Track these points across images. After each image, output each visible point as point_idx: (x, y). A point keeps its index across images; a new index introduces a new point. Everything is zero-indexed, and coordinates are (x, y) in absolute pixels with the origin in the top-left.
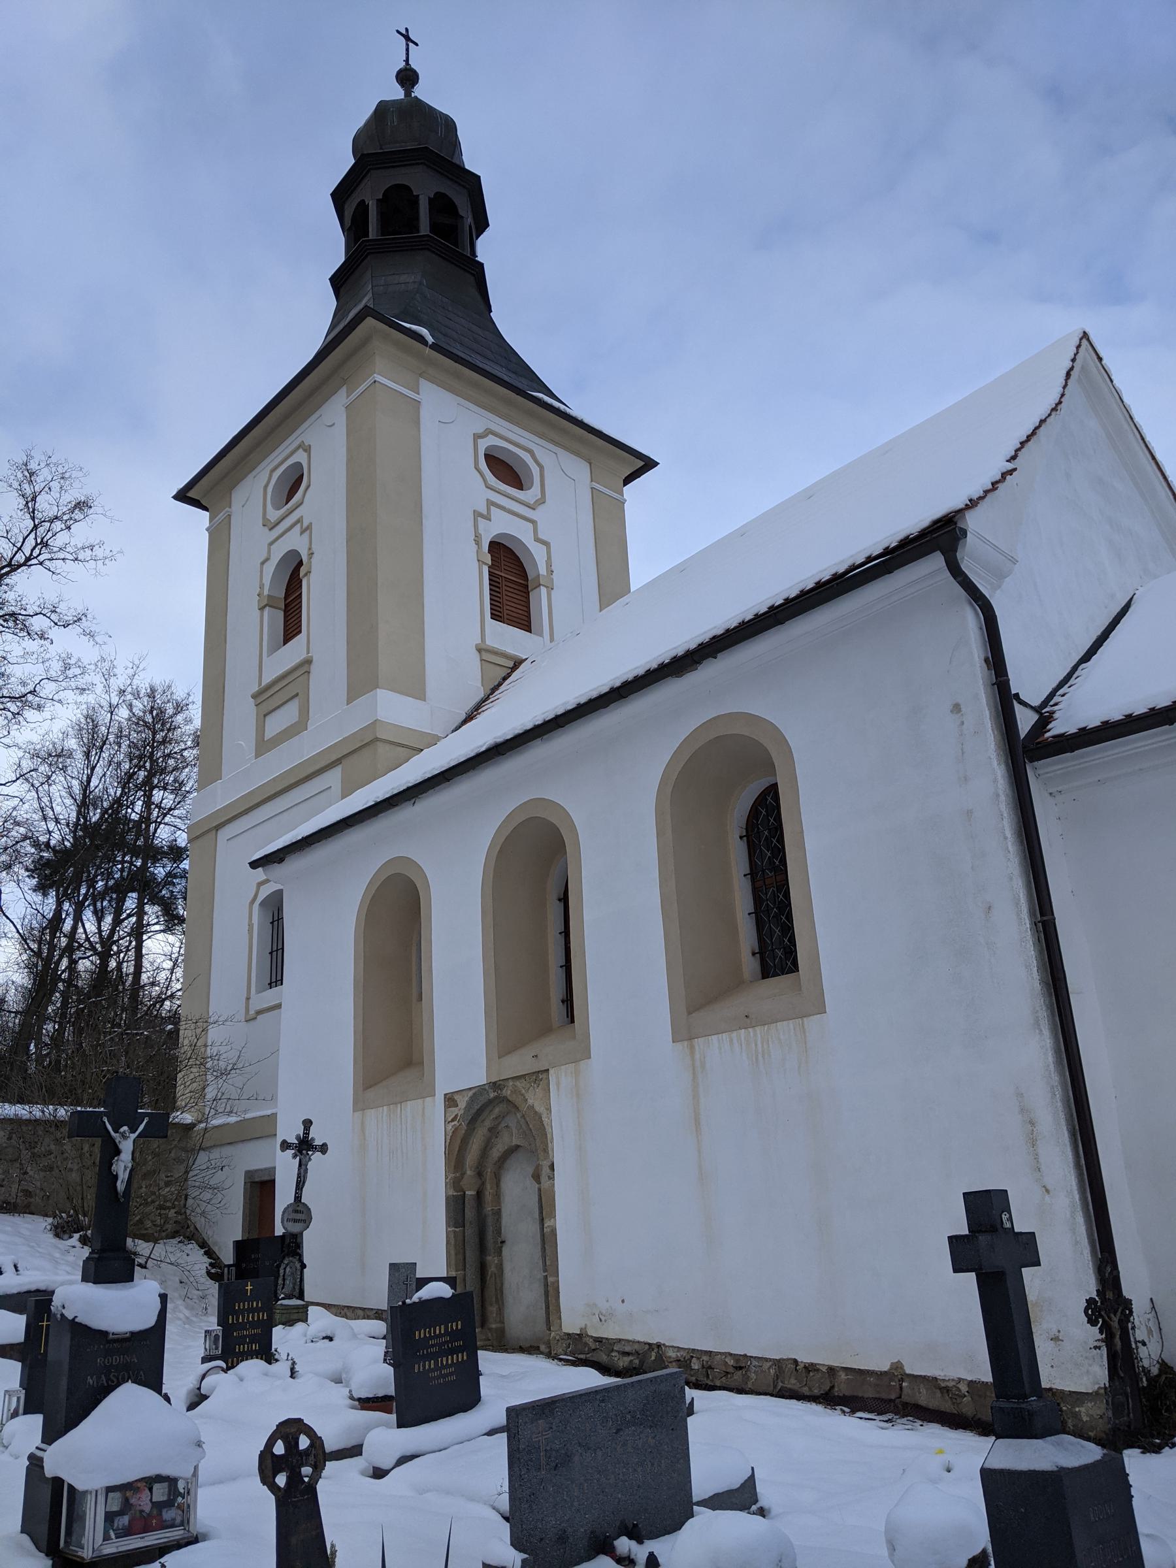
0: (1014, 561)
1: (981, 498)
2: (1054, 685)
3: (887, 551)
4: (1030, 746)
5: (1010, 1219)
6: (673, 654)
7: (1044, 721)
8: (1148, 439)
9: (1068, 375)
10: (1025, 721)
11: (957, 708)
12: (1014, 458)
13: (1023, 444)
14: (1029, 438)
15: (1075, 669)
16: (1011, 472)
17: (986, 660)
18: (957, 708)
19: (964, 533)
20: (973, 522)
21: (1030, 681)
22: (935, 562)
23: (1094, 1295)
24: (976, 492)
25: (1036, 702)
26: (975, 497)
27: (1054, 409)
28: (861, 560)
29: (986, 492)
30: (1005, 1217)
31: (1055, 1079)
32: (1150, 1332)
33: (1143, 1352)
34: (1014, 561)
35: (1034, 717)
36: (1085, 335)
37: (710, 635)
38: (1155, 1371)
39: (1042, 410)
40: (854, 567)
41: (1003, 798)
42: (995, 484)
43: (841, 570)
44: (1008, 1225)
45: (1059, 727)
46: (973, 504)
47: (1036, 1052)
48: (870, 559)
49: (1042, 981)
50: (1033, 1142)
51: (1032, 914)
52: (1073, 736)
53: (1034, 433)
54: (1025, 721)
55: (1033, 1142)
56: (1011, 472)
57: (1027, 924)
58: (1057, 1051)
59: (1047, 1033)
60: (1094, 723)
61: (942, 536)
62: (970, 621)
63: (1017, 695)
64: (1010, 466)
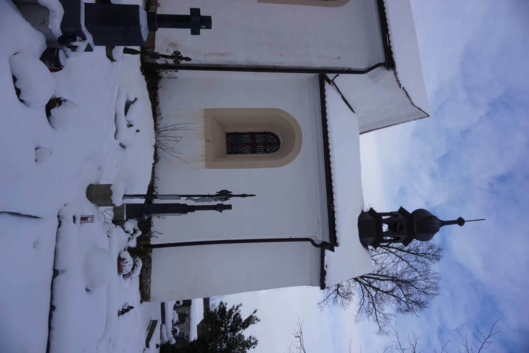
0: (375, 83)
1: (396, 77)
2: (338, 87)
3: (390, 47)
4: (323, 76)
5: (204, 28)
6: (386, 8)
7: (329, 82)
8: (395, 126)
9: (420, 109)
10: (331, 76)
11: (339, 58)
12: (403, 89)
13: (406, 92)
14: (407, 94)
15: (341, 93)
16: (400, 87)
17: (350, 69)
18: (339, 58)
19: (388, 70)
20: (391, 73)
21: (342, 80)
22: (382, 60)
23: (181, 54)
24: (398, 76)
25: (335, 81)
26: (397, 75)
27: (412, 103)
28: (390, 39)
29: (397, 79)
30: (204, 27)
31: (234, 64)
32: (169, 75)
33: (165, 72)
34: (375, 83)
35: (331, 79)
36: (428, 116)
37: (393, 52)
38: (160, 75)
39: (413, 100)
40: (389, 36)
41: (311, 65)
42: (398, 81)
43: (389, 32)
44: (202, 27)
45: (327, 86)
46: (396, 74)
47: (241, 60)
48: (390, 41)
49: (260, 66)
50: (218, 54)
51: (278, 67)
52: (324, 88)
53: (408, 96)
54: (331, 76)
55: (218, 54)
56: (400, 87)
57: (276, 65)
58: (241, 66)
59: (246, 64)
60: (326, 93)
61: (389, 63)
62: (363, 66)
63: (338, 75)
64: (402, 87)
